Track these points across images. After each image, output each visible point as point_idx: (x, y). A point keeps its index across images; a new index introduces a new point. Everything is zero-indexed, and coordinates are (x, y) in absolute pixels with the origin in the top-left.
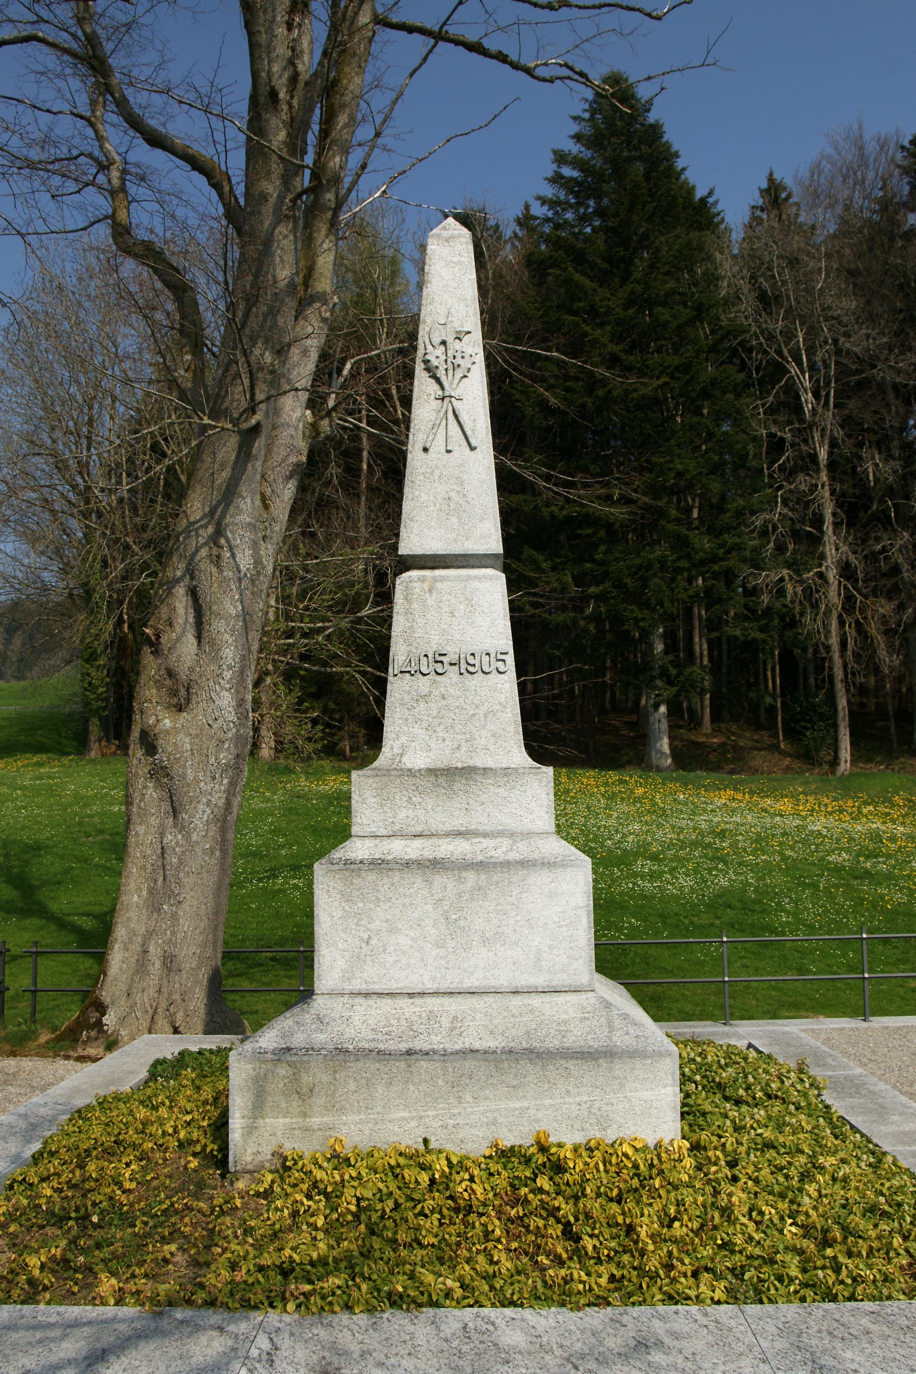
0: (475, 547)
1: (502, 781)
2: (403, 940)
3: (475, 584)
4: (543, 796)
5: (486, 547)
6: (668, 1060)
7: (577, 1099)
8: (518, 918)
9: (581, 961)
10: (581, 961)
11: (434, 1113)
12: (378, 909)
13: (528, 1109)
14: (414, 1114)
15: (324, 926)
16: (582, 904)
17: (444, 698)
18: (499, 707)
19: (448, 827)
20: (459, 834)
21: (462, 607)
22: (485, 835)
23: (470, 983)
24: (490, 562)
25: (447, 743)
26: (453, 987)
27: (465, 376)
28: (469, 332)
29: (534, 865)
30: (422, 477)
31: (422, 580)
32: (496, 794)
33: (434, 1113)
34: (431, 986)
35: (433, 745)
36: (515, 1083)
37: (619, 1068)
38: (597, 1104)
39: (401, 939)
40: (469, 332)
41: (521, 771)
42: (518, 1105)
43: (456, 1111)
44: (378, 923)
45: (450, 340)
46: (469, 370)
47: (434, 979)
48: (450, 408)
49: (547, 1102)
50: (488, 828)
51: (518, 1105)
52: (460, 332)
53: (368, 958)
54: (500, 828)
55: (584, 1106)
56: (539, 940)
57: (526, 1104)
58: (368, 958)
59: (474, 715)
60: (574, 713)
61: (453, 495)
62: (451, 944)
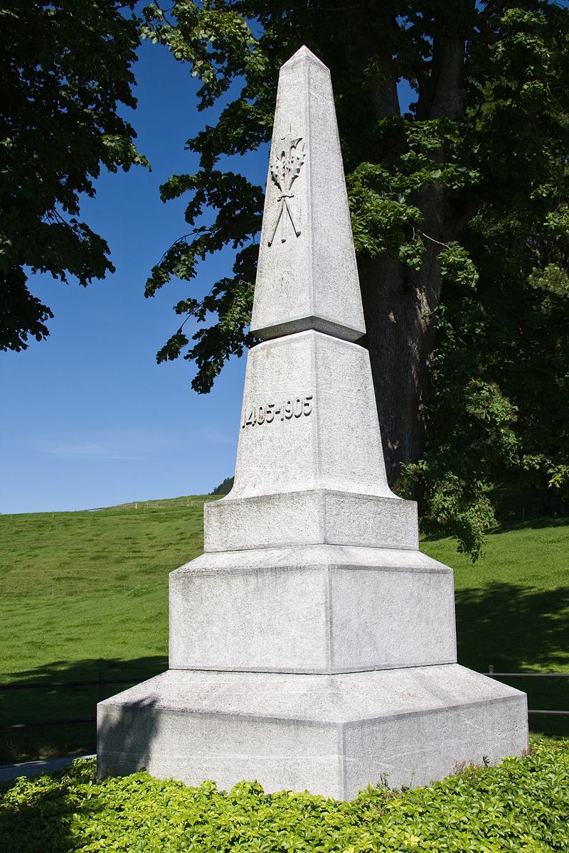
1: (290, 503)
3: (295, 345)
4: (316, 513)
5: (303, 313)
6: (335, 732)
8: (282, 613)
9: (321, 649)
10: (321, 649)
11: (196, 757)
12: (202, 606)
13: (247, 761)
14: (185, 757)
15: (174, 618)
16: (321, 602)
18: (303, 443)
19: (257, 543)
20: (264, 547)
22: (279, 547)
23: (253, 664)
24: (305, 326)
25: (272, 476)
26: (243, 666)
27: (296, 177)
28: (301, 139)
29: (291, 569)
31: (263, 349)
33: (196, 757)
34: (232, 666)
35: (262, 479)
36: (240, 739)
37: (303, 733)
39: (215, 629)
40: (301, 139)
43: (207, 758)
44: (202, 617)
45: (287, 150)
46: (298, 171)
47: (232, 660)
48: (285, 205)
49: (259, 757)
50: (281, 542)
54: (289, 541)
55: (282, 763)
56: (294, 631)
57: (247, 758)
60: (426, 444)
61: (285, 276)
62: (242, 633)
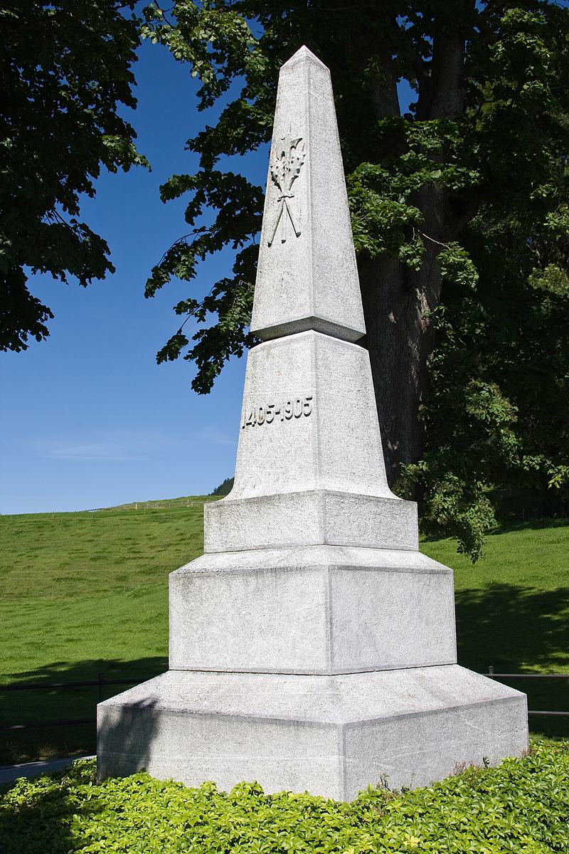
0: (297, 315)
2: (215, 630)
3: (295, 345)
6: (334, 733)
7: (277, 758)
13: (247, 762)
16: (322, 602)
17: (271, 441)
18: (303, 444)
21: (286, 365)
22: (279, 548)
23: (253, 665)
25: (271, 476)
26: (243, 667)
27: (296, 177)
28: (301, 139)
29: (291, 570)
30: (267, 267)
31: (262, 349)
32: (286, 515)
33: (196, 758)
34: (232, 667)
36: (240, 740)
37: (304, 734)
38: (289, 764)
41: (302, 494)
42: (242, 758)
45: (287, 150)
46: (298, 171)
47: (232, 661)
51: (242, 758)
52: (294, 141)
53: (197, 644)
54: (289, 542)
58: (197, 644)
59: (289, 452)
60: (426, 444)
61: (285, 276)
